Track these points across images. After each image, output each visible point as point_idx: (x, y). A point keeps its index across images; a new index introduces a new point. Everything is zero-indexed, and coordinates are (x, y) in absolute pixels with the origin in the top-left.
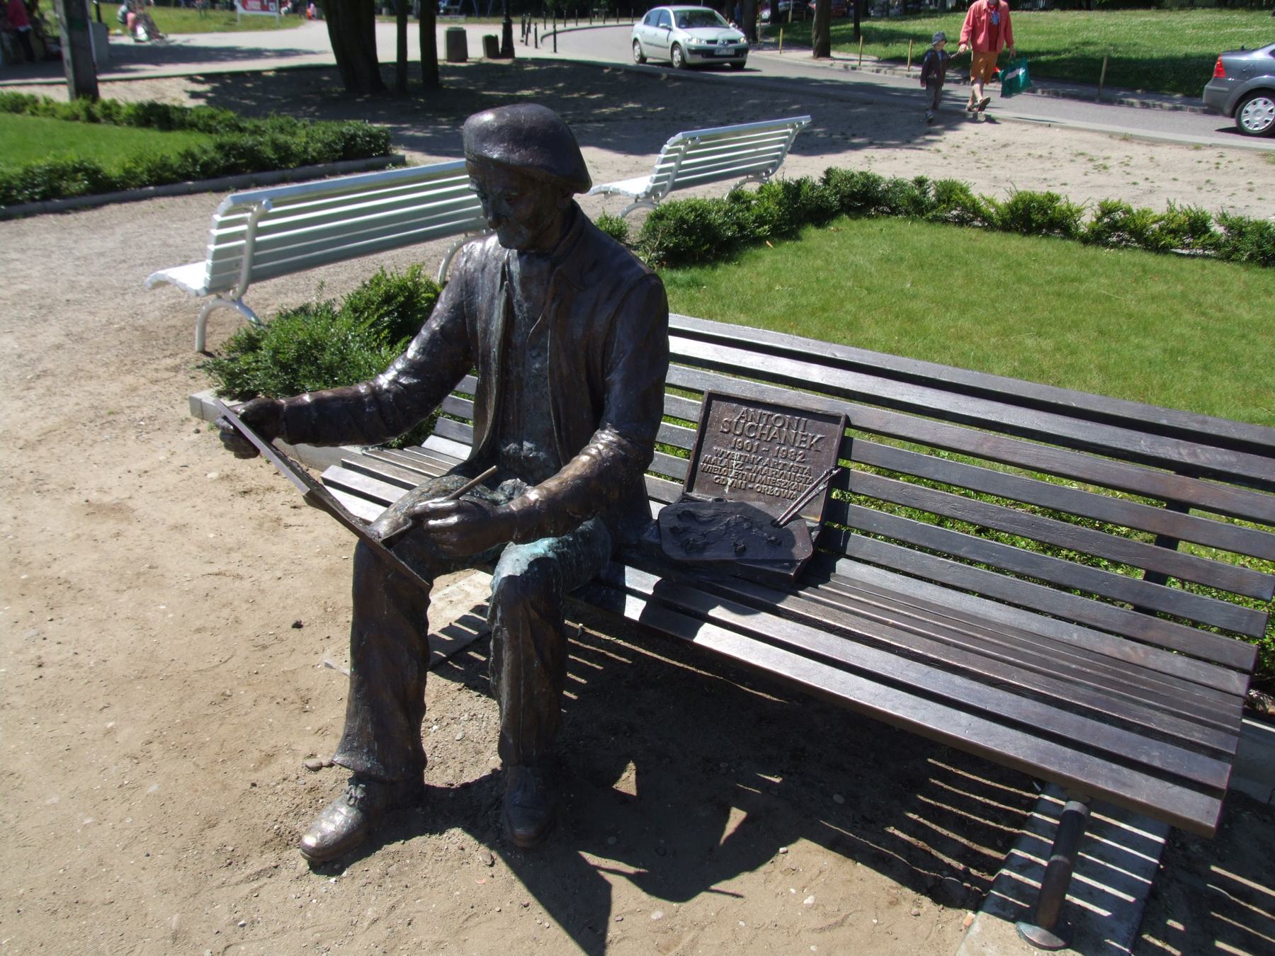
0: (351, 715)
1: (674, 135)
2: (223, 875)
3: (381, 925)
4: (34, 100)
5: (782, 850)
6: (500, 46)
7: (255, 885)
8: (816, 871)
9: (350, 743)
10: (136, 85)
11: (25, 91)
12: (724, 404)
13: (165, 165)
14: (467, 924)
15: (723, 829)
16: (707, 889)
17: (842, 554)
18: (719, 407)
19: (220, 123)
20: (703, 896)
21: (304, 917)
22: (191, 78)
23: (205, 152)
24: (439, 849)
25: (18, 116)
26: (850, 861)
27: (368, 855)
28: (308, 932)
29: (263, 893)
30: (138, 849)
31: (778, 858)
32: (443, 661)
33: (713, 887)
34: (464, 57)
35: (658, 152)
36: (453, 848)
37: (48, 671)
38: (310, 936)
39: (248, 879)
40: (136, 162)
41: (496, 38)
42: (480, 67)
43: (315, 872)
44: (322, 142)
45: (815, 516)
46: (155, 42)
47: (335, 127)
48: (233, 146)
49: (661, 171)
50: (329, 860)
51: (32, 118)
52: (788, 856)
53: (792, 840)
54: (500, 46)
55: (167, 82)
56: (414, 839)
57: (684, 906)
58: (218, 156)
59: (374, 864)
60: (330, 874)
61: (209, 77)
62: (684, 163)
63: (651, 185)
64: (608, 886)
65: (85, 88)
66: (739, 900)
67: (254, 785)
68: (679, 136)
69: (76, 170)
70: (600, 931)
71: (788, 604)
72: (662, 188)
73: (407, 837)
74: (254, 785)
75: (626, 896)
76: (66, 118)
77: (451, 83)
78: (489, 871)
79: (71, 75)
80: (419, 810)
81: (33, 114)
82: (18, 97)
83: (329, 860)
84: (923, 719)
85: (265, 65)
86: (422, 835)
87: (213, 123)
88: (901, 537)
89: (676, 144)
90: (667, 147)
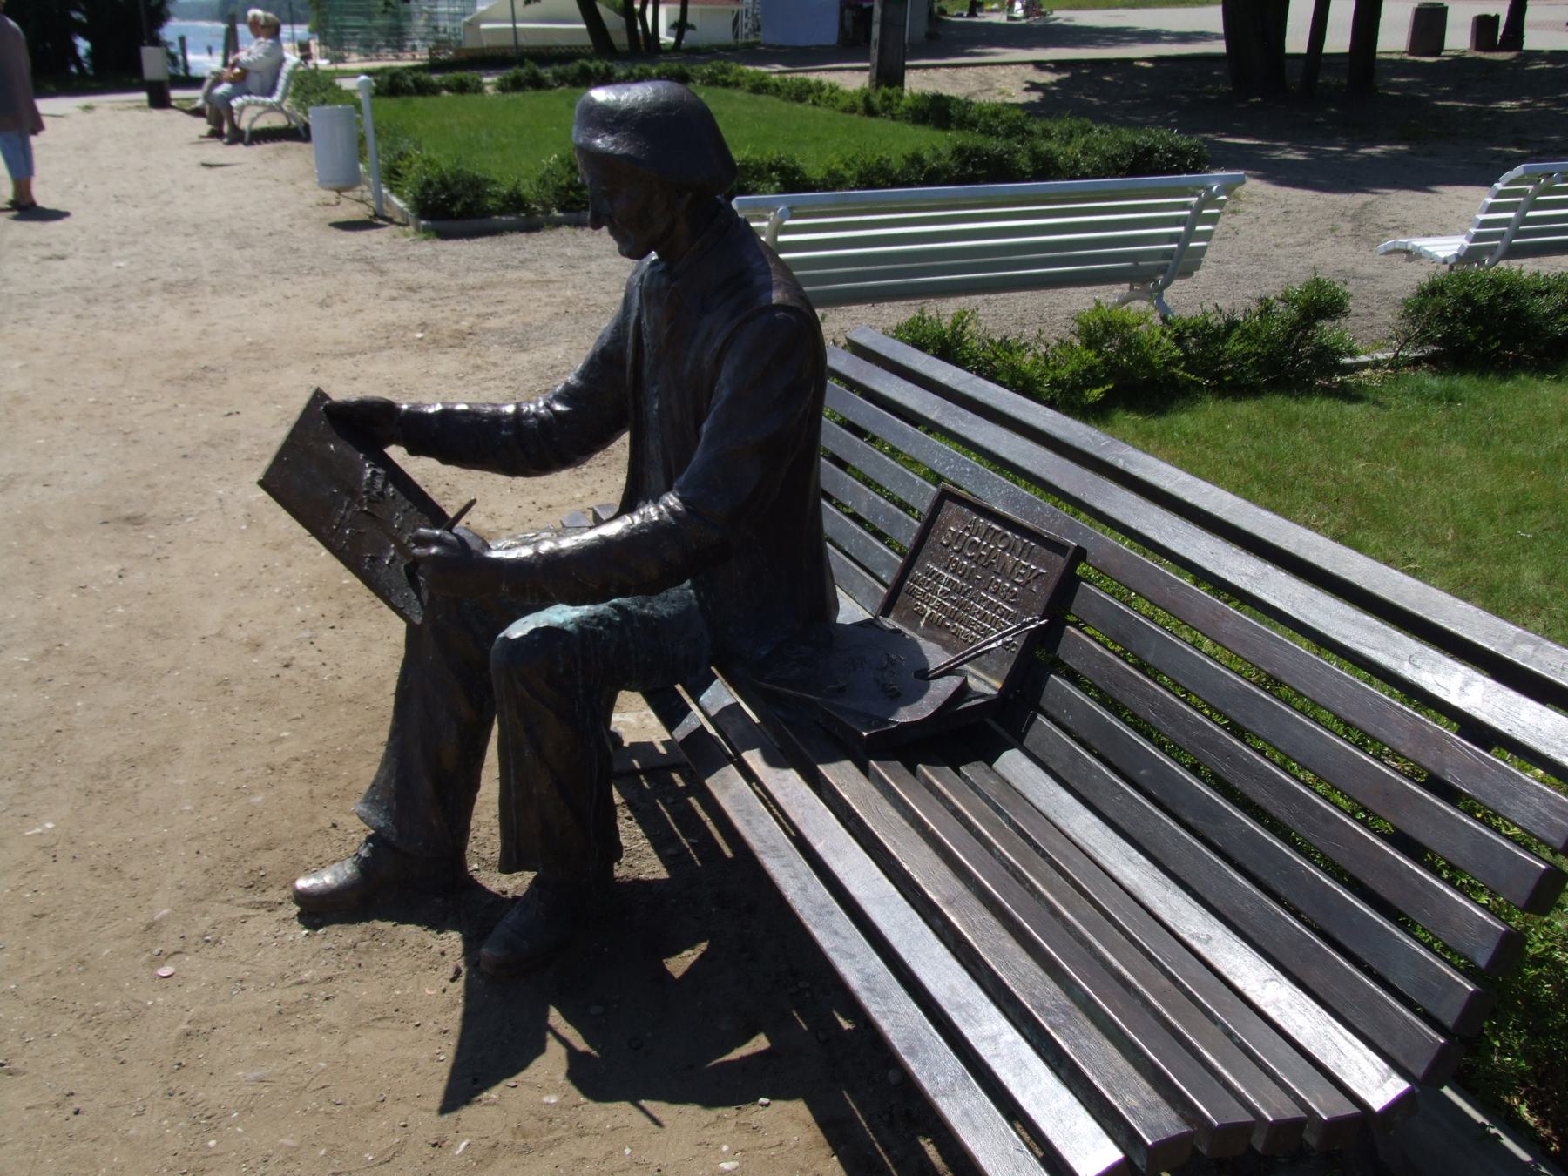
0: (385, 762)
1: (1511, 169)
2: (234, 893)
3: (304, 989)
4: (820, 86)
5: (763, 1100)
6: (1500, 32)
7: (251, 912)
8: (777, 1140)
9: (374, 797)
10: (963, 73)
11: (813, 77)
12: (955, 507)
13: (881, 169)
14: (380, 1024)
15: (730, 1050)
16: (635, 1102)
17: (1017, 741)
18: (950, 510)
19: (1002, 123)
20: (625, 1105)
21: (253, 956)
22: (1040, 65)
23: (938, 157)
24: (422, 945)
25: (799, 106)
26: (828, 1149)
27: (352, 923)
28: (243, 968)
29: (250, 924)
30: (195, 845)
31: (749, 1109)
32: (636, 773)
33: (643, 1103)
34: (1438, 48)
35: (1490, 184)
36: (436, 948)
37: (288, 673)
38: (243, 972)
39: (249, 905)
40: (847, 165)
41: (1497, 17)
42: (1460, 63)
43: (300, 921)
44: (1102, 154)
45: (994, 675)
46: (1035, 20)
47: (1127, 135)
48: (977, 151)
49: (1484, 224)
50: (317, 911)
51: (810, 109)
52: (763, 1112)
53: (788, 1096)
54: (1500, 32)
55: (1002, 71)
56: (408, 926)
57: (592, 1104)
58: (953, 164)
59: (351, 934)
60: (307, 926)
61: (1059, 65)
62: (1530, 214)
63: (1467, 244)
64: (540, 1049)
65: (890, 76)
66: (655, 1128)
67: (334, 826)
68: (1519, 170)
69: (772, 168)
70: (478, 1086)
71: (842, 775)
72: (1490, 251)
73: (403, 920)
74: (334, 826)
75: (551, 1065)
76: (844, 110)
77: (1396, 87)
78: (446, 983)
79: (875, 58)
80: (438, 900)
81: (814, 103)
82: (806, 83)
83: (317, 911)
84: (835, 949)
85: (1138, 51)
86: (419, 924)
87: (994, 122)
88: (1085, 736)
89: (1511, 183)
90: (1498, 186)
